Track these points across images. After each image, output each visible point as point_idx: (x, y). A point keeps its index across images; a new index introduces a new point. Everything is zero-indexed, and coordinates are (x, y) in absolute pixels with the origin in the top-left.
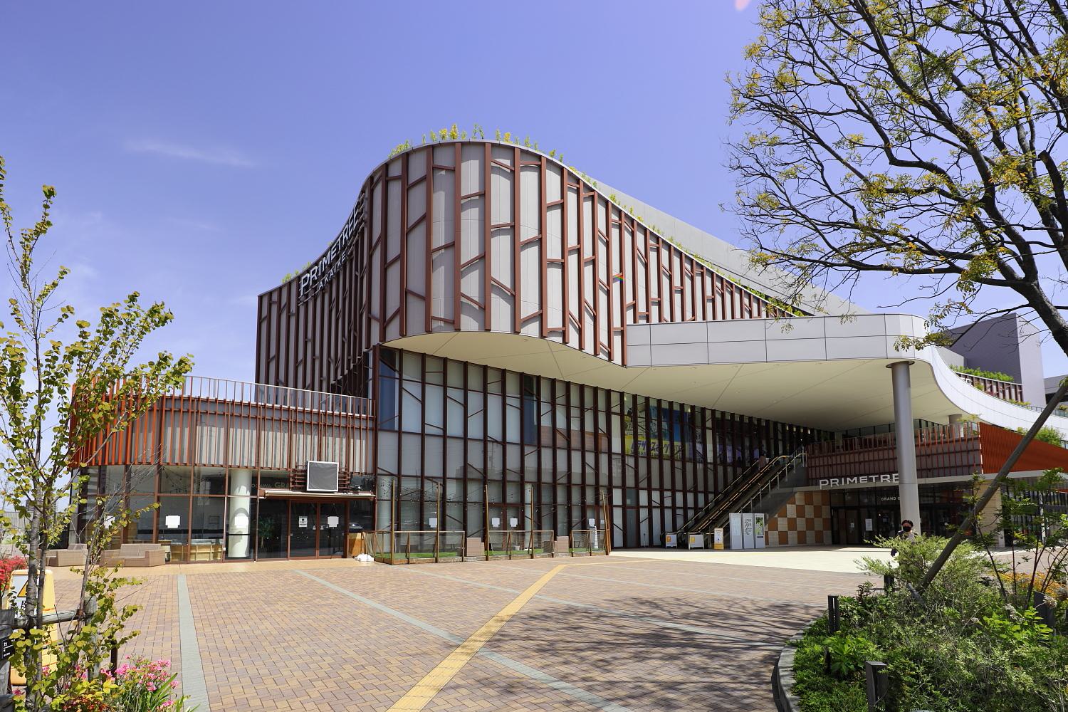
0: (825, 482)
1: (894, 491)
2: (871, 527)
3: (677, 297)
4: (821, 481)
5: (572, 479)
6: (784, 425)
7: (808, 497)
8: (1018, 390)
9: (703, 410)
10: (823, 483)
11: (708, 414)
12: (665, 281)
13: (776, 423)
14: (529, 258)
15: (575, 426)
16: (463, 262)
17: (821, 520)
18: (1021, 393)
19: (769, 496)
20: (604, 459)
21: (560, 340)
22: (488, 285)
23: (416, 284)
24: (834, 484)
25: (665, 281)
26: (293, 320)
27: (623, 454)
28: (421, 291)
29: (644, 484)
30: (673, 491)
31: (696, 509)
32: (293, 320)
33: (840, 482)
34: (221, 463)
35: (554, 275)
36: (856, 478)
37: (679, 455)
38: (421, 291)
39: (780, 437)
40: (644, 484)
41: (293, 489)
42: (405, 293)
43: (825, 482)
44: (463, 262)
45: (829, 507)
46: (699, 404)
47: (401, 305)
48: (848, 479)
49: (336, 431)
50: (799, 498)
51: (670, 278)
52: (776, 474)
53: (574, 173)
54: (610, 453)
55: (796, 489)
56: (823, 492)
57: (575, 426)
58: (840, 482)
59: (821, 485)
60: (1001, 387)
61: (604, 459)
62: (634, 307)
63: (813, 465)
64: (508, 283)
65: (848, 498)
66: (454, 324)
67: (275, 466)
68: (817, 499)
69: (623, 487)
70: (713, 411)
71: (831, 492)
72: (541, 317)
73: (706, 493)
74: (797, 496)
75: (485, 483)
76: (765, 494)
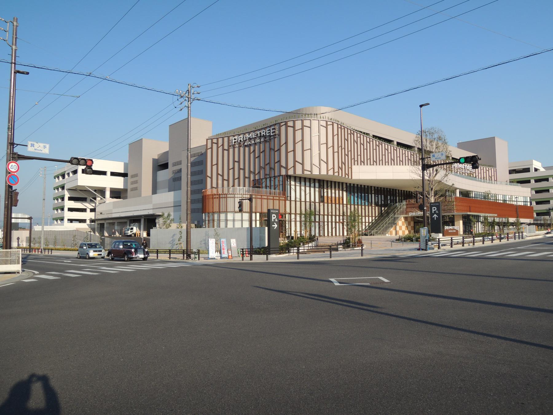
0: (411, 214)
2: (231, 241)
3: (365, 151)
4: (410, 213)
7: (406, 219)
9: (371, 187)
10: (410, 214)
15: (333, 195)
17: (410, 226)
20: (341, 206)
26: (353, 157)
28: (210, 176)
30: (369, 217)
31: (369, 223)
32: (353, 157)
38: (210, 176)
39: (397, 195)
42: (295, 161)
43: (411, 214)
45: (413, 222)
51: (363, 145)
53: (7, 193)
54: (343, 204)
56: (411, 217)
57: (333, 195)
59: (410, 214)
61: (341, 206)
68: (409, 220)
70: (375, 187)
73: (372, 217)
75: (233, 220)
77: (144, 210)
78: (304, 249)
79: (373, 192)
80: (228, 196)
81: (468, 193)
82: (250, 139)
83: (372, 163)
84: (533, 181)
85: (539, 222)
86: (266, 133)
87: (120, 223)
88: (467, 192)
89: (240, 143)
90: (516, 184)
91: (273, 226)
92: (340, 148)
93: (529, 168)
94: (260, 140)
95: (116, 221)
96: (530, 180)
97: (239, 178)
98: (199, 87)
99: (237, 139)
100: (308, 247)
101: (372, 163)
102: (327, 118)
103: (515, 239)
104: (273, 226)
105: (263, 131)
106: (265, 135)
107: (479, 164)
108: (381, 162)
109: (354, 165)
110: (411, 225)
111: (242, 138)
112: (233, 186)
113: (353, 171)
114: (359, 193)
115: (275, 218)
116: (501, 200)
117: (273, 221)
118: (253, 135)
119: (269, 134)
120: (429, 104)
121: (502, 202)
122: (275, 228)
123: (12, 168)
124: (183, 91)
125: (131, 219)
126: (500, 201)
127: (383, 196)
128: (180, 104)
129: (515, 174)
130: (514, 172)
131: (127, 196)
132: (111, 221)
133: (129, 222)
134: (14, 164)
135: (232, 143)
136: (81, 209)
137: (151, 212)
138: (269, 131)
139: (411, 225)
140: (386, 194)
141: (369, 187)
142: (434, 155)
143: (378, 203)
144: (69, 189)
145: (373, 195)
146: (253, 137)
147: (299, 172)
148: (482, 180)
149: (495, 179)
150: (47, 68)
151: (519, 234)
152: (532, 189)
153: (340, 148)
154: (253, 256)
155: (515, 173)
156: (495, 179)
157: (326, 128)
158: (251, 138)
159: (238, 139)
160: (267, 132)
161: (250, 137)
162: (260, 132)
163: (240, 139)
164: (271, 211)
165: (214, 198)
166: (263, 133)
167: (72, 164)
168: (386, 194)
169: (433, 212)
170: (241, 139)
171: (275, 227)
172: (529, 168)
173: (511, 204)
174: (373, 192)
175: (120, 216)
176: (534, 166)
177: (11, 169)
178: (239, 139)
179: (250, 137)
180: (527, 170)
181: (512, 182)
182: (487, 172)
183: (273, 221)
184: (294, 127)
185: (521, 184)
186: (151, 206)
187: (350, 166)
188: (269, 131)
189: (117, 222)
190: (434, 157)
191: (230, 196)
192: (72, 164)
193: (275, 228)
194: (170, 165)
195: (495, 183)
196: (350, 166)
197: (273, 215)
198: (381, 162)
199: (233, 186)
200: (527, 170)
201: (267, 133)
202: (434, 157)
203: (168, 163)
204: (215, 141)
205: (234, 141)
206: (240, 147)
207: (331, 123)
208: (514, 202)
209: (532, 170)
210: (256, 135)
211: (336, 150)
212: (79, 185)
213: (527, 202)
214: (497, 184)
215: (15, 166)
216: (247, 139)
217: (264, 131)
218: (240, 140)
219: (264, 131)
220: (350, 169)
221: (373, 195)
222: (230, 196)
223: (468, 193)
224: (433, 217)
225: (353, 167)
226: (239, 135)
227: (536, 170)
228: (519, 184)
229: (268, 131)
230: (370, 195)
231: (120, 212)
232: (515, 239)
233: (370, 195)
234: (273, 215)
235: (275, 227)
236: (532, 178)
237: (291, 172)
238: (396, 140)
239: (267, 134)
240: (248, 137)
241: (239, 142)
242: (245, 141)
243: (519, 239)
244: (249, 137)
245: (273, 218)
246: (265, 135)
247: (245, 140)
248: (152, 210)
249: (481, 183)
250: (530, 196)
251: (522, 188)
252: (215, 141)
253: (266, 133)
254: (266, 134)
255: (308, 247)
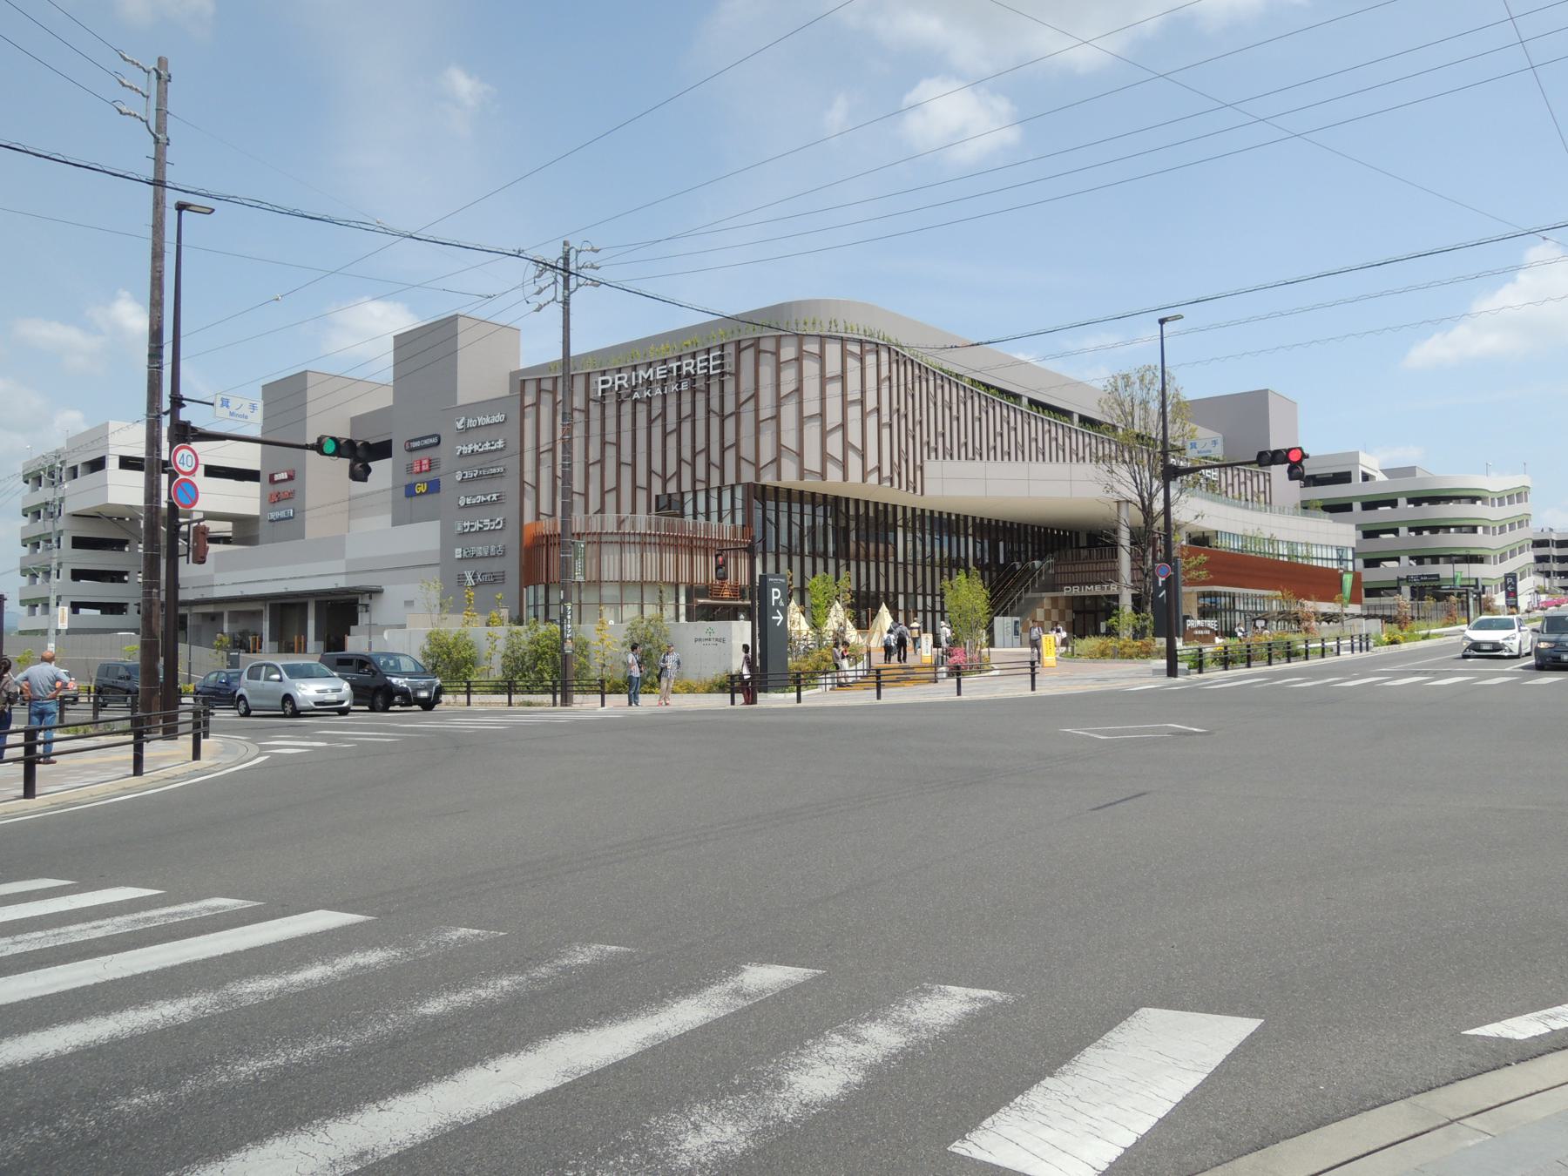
1: (1116, 598)
5: (180, 573)
6: (1033, 527)
7: (1054, 601)
8: (1267, 478)
9: (966, 517)
11: (970, 519)
12: (947, 412)
13: (1026, 526)
14: (872, 422)
16: (782, 396)
18: (1270, 480)
19: (1023, 601)
21: (889, 484)
22: (846, 445)
23: (789, 440)
24: (1075, 591)
25: (947, 412)
27: (905, 564)
29: (920, 590)
33: (1080, 590)
34: (617, 579)
35: (886, 432)
36: (1092, 587)
37: (929, 560)
40: (920, 590)
41: (711, 599)
44: (782, 396)
46: (963, 513)
47: (777, 454)
48: (1087, 587)
49: (632, 546)
50: (1047, 603)
51: (950, 409)
52: (1028, 581)
55: (1044, 594)
58: (1080, 590)
60: (1249, 474)
62: (928, 443)
63: (1059, 571)
64: (859, 446)
65: (1088, 602)
66: (823, 475)
67: (661, 579)
68: (1062, 603)
69: (905, 593)
70: (974, 518)
71: (1074, 598)
72: (879, 469)
74: (1045, 600)
76: (1019, 599)
77: (274, 580)
78: (857, 677)
79: (970, 531)
80: (604, 539)
81: (1206, 535)
82: (648, 382)
83: (970, 455)
84: (1357, 506)
85: (1387, 613)
86: (695, 366)
87: (235, 615)
88: (1203, 533)
89: (618, 395)
90: (1322, 513)
91: (774, 618)
92: (895, 417)
93: (1349, 474)
94: (679, 387)
95: (226, 610)
96: (1351, 505)
97: (617, 489)
98: (597, 251)
99: (611, 383)
100: (856, 670)
101: (970, 455)
102: (861, 332)
103: (1353, 652)
104: (774, 618)
105: (688, 361)
106: (693, 372)
107: (1305, 468)
108: (992, 453)
109: (929, 458)
110: (1067, 620)
111: (626, 380)
112: (602, 510)
113: (925, 476)
114: (945, 533)
115: (778, 598)
116: (1283, 555)
117: (773, 604)
118: (658, 373)
119: (706, 371)
120: (1182, 317)
121: (1286, 559)
122: (778, 624)
123: (183, 464)
124: (553, 255)
125: (274, 602)
126: (1281, 558)
127: (986, 542)
128: (535, 294)
129: (1312, 488)
130: (1312, 482)
131: (258, 536)
132: (210, 609)
133: (268, 611)
134: (186, 452)
135: (597, 393)
136: (116, 571)
137: (342, 583)
138: (706, 364)
139: (1067, 620)
140: (993, 536)
141: (962, 518)
142: (1195, 444)
143: (983, 560)
144: (74, 515)
145: (970, 539)
146: (658, 377)
147: (789, 478)
148: (1250, 507)
149: (1268, 501)
150: (100, 169)
151: (1352, 641)
152: (1358, 527)
153: (895, 417)
154: (736, 695)
155: (1314, 485)
156: (1268, 501)
157: (862, 360)
158: (651, 379)
159: (614, 383)
160: (699, 365)
161: (649, 377)
162: (679, 363)
163: (620, 382)
164: (770, 580)
165: (551, 544)
166: (688, 368)
167: (321, 454)
168: (993, 536)
169: (1160, 585)
170: (624, 382)
171: (778, 620)
172: (1349, 474)
173: (1307, 565)
174: (970, 531)
175: (205, 597)
176: (1361, 468)
177: (180, 466)
178: (617, 382)
179: (649, 377)
180: (1344, 478)
181: (1306, 506)
182: (686, 454)
183: (773, 604)
184: (777, 354)
185: (1331, 512)
186: (339, 566)
187: (918, 462)
188: (706, 364)
189: (230, 612)
190: (1196, 448)
191: (610, 538)
192: (322, 453)
193: (778, 624)
194: (397, 448)
195: (1266, 511)
196: (918, 462)
197: (774, 590)
198: (992, 453)
199: (602, 510)
200: (1344, 478)
201: (698, 368)
202: (1196, 448)
203: (390, 442)
204: (547, 385)
205: (601, 387)
206: (619, 403)
207: (874, 346)
208: (1330, 562)
209: (1357, 479)
210: (665, 371)
211: (885, 419)
212: (109, 502)
213: (1347, 560)
214: (1271, 512)
215: (190, 458)
216: (640, 382)
217: (690, 363)
218: (620, 386)
219: (690, 363)
220: (919, 473)
221: (970, 539)
222: (610, 538)
223: (1206, 535)
224: (1160, 596)
225: (927, 464)
226: (619, 370)
227: (1366, 477)
228: (1328, 514)
229: (714, 359)
230: (962, 540)
231: (288, 577)
232: (1353, 652)
233: (962, 540)
234: (774, 590)
235: (778, 620)
236: (1356, 498)
237: (768, 479)
238: (1027, 393)
239: (699, 372)
240: (643, 378)
241: (616, 389)
242: (634, 389)
243: (1361, 651)
244: (646, 377)
245: (774, 598)
246: (693, 372)
247: (634, 384)
248: (344, 576)
249: (1246, 511)
250: (1354, 546)
251: (1335, 524)
252: (547, 385)
253: (695, 366)
254: (696, 371)
255: (856, 670)
